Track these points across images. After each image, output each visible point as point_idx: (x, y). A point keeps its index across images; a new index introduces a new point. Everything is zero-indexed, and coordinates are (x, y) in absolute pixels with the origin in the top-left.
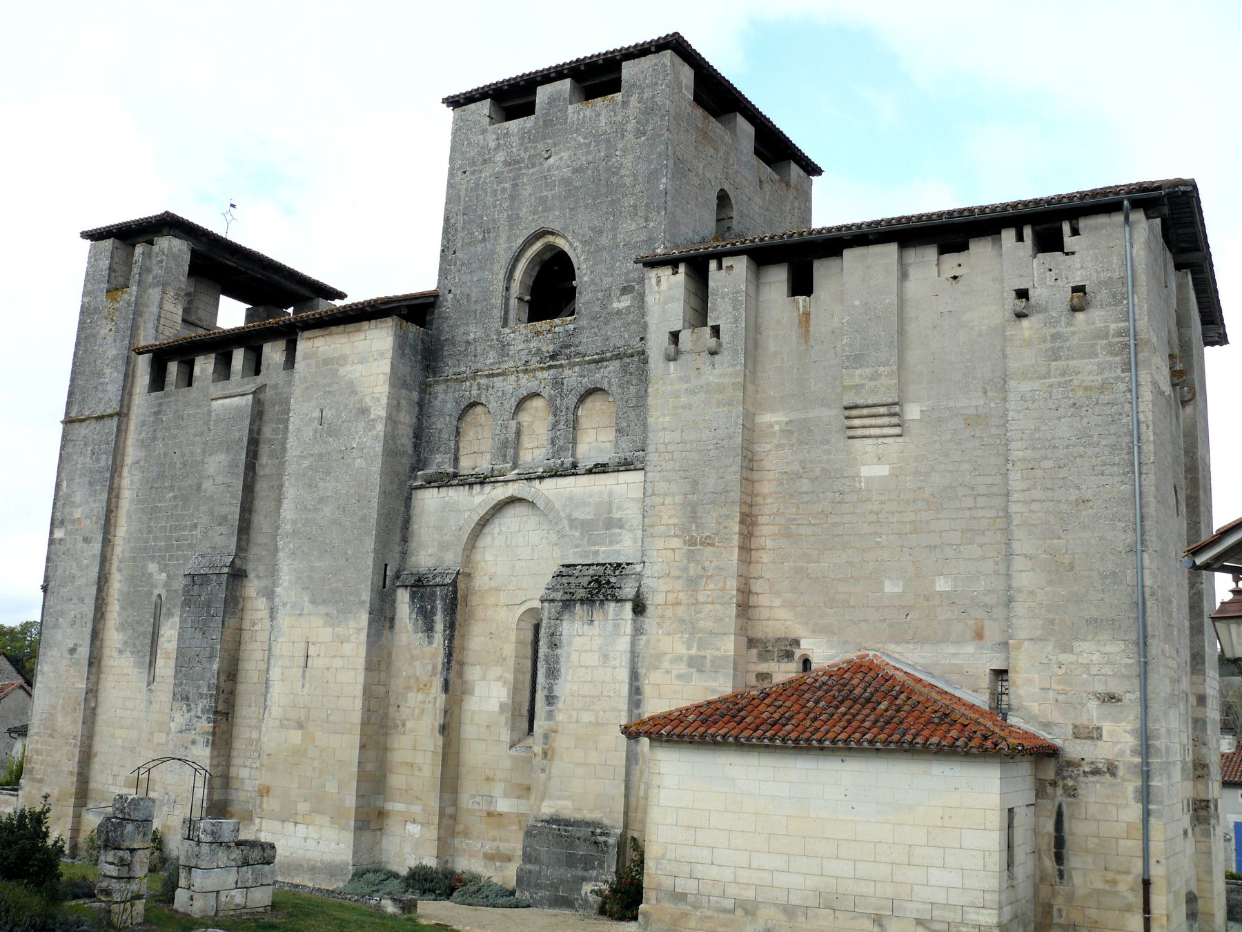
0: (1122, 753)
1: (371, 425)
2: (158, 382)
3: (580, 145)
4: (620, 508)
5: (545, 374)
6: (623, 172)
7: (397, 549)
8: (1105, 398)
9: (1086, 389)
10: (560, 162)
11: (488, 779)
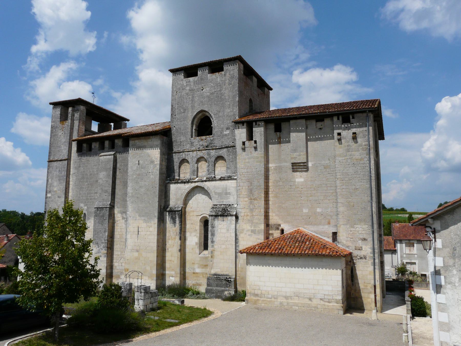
0: (368, 253)
1: (155, 166)
2: (79, 150)
3: (212, 86)
4: (229, 189)
5: (205, 151)
6: (225, 95)
7: (163, 200)
8: (362, 162)
9: (356, 160)
10: (207, 91)
11: (193, 263)
